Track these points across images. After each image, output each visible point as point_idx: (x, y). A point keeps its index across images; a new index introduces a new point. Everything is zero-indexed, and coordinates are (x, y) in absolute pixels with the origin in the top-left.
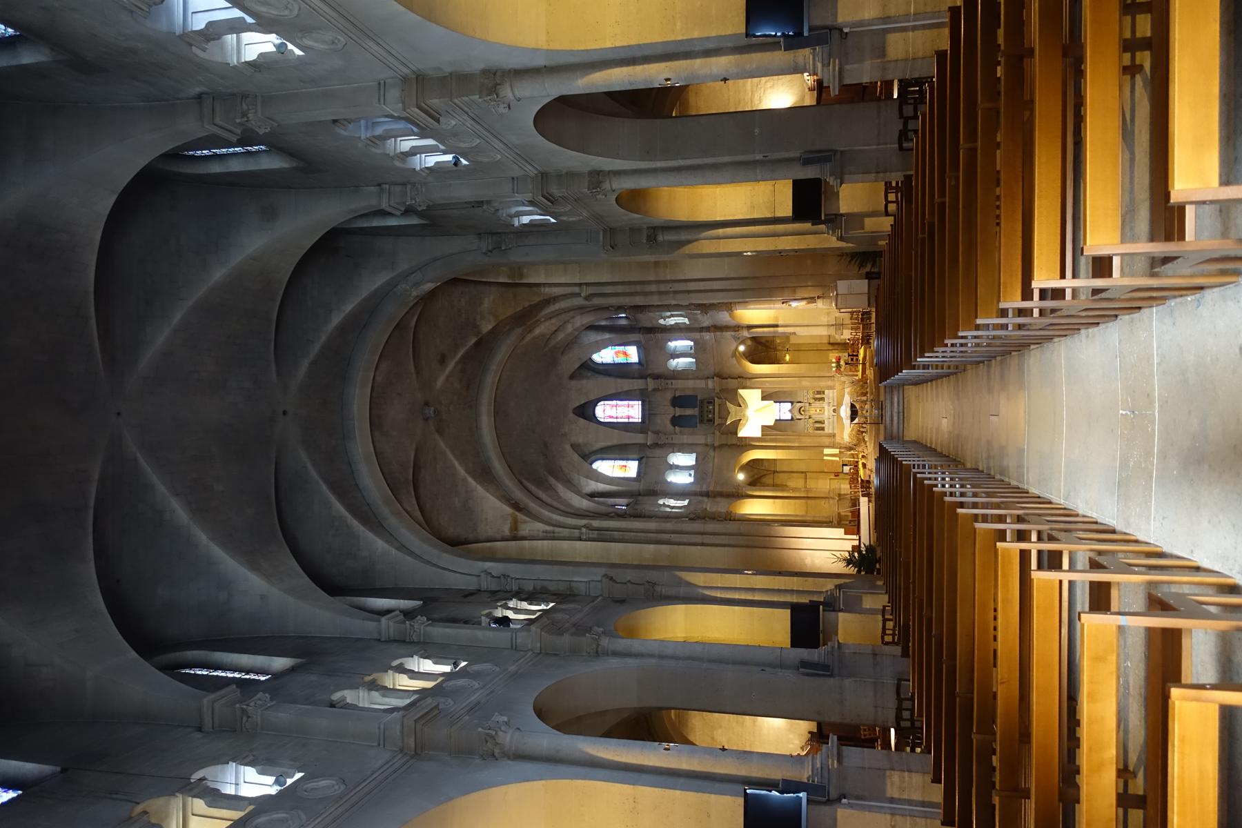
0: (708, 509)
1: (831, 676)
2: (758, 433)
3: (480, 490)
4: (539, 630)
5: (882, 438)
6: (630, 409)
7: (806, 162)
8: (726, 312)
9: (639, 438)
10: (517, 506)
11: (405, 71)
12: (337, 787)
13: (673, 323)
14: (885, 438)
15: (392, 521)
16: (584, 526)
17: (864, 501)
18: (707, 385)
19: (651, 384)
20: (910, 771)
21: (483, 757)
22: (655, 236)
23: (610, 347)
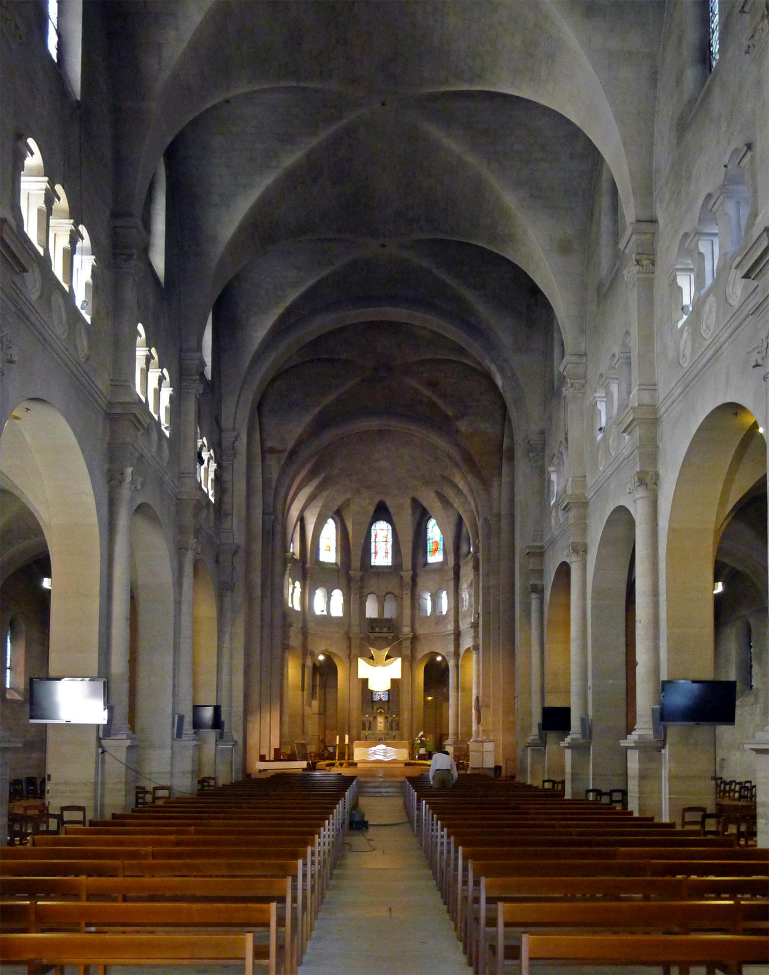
0: (292, 628)
1: (173, 739)
2: (361, 675)
3: (307, 419)
4: (197, 498)
5: (361, 779)
6: (384, 554)
7: (584, 721)
8: (472, 644)
9: (356, 563)
10: (294, 452)
11: (663, 410)
12: (83, 355)
13: (463, 595)
14: (361, 782)
15: (282, 346)
16: (276, 518)
17: (303, 764)
18: (406, 626)
19: (407, 575)
20: (126, 795)
21: (109, 471)
22: (536, 592)
23: (442, 536)
